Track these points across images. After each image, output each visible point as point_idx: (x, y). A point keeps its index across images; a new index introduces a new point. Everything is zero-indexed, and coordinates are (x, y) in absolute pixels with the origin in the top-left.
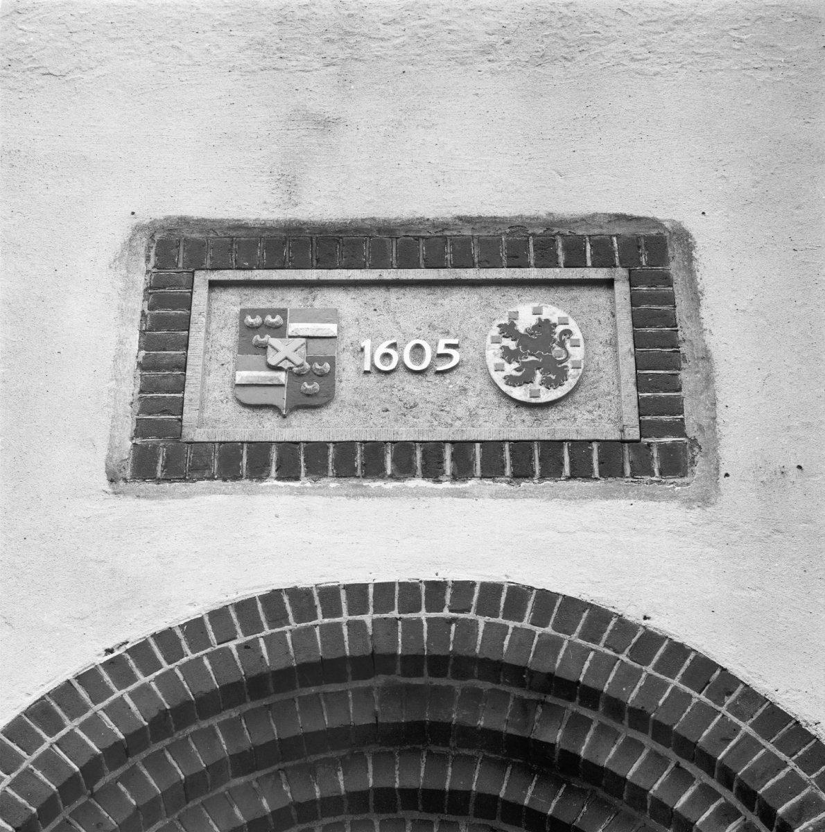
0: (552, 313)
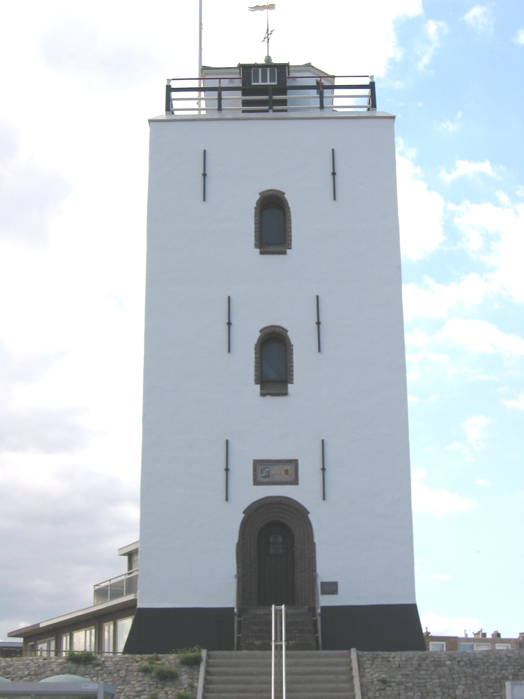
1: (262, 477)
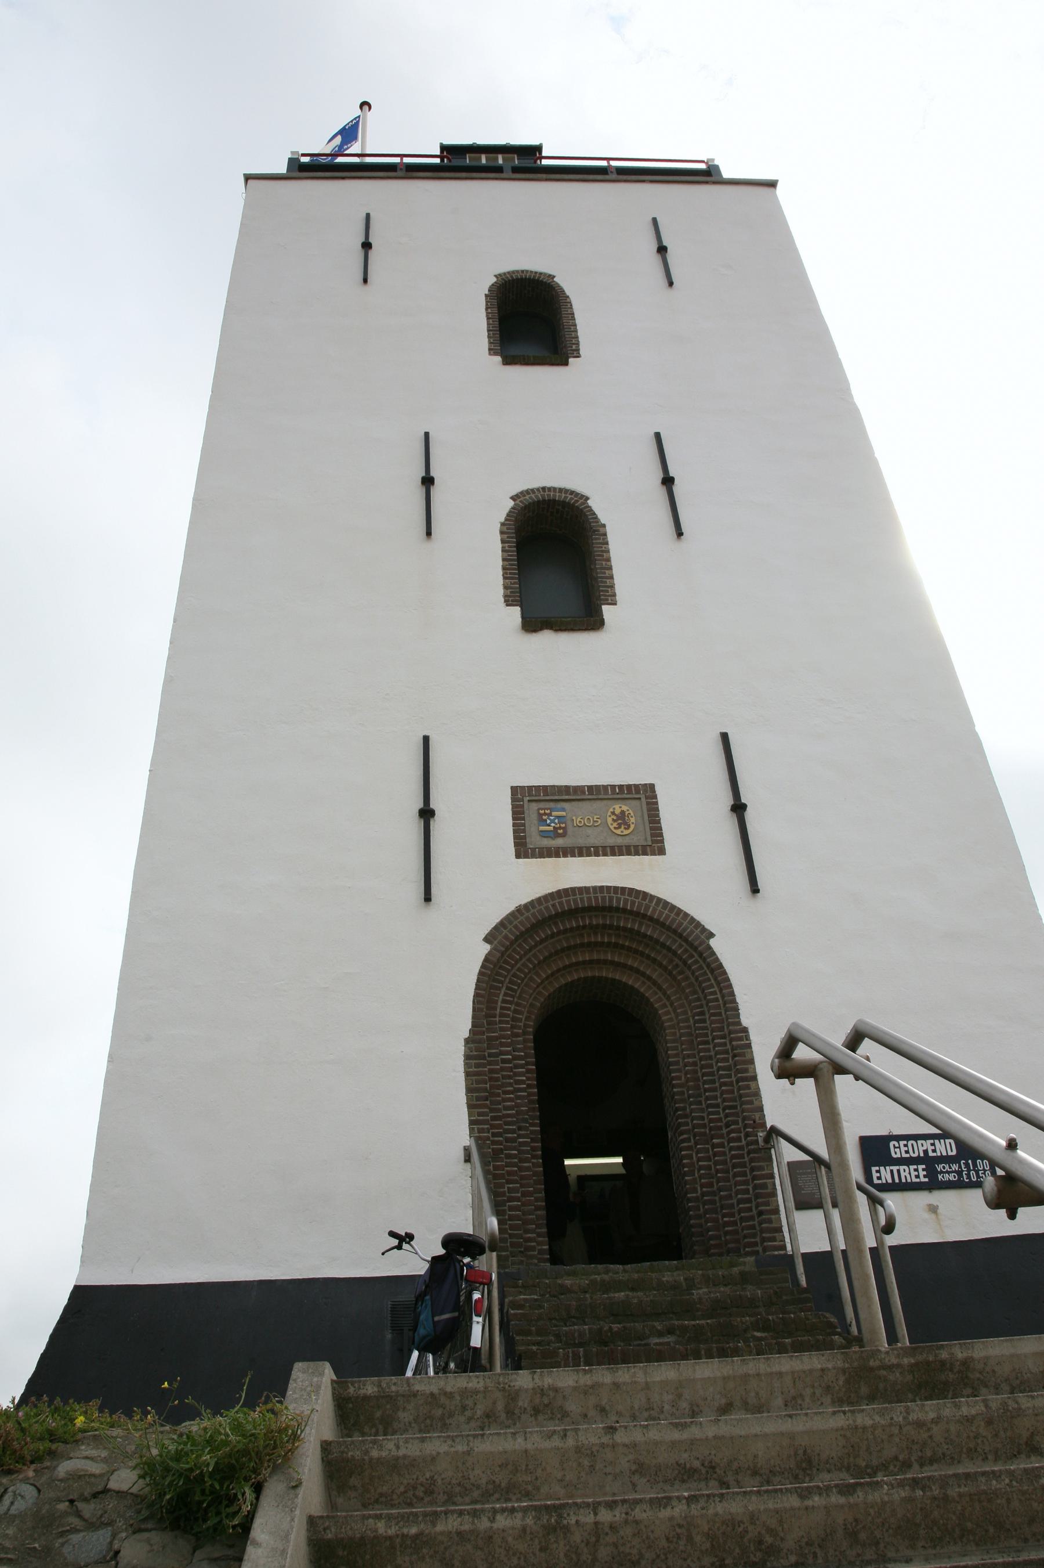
0: (625, 808)
1: (544, 834)
